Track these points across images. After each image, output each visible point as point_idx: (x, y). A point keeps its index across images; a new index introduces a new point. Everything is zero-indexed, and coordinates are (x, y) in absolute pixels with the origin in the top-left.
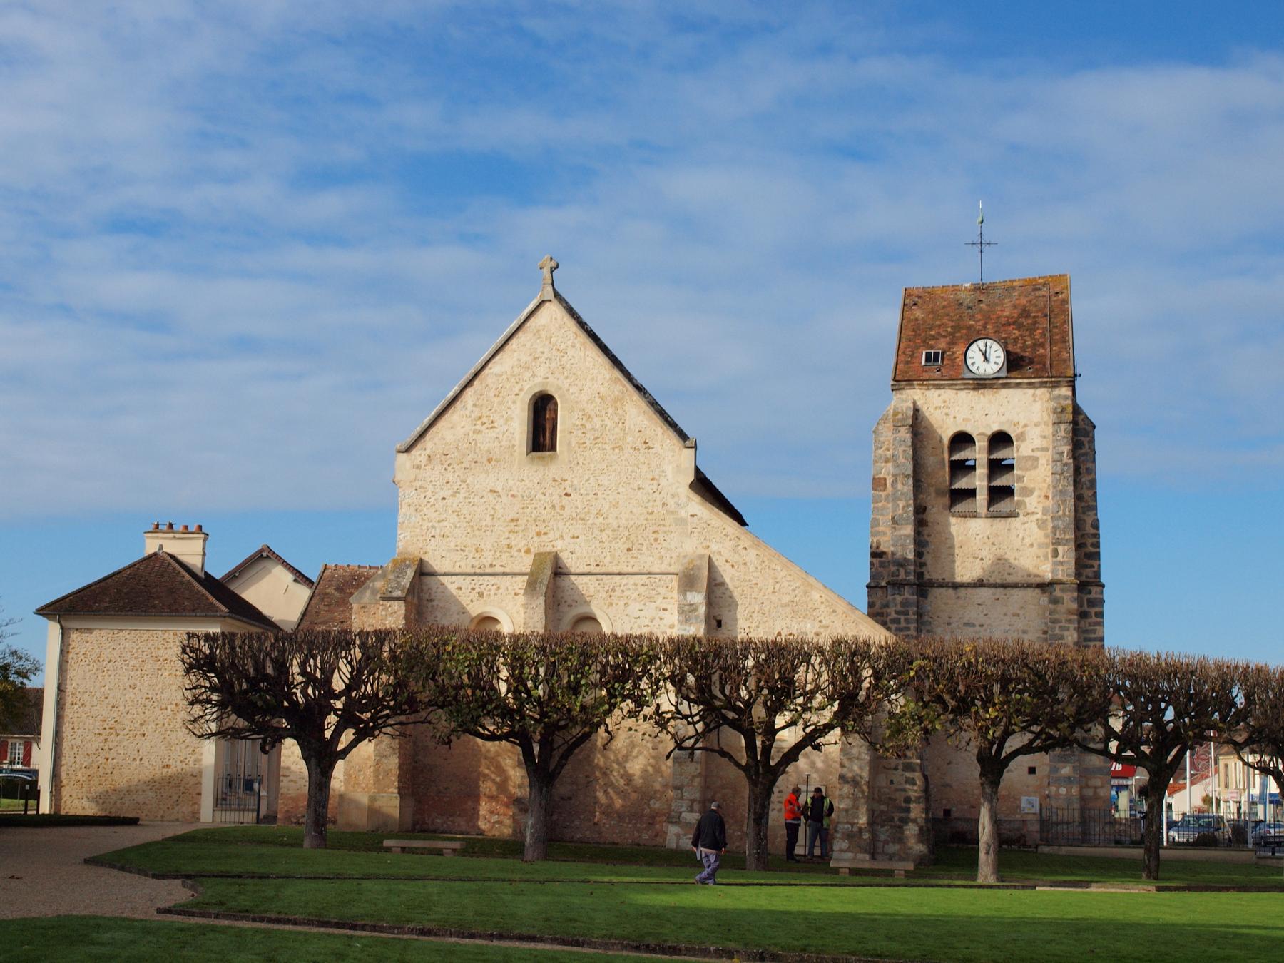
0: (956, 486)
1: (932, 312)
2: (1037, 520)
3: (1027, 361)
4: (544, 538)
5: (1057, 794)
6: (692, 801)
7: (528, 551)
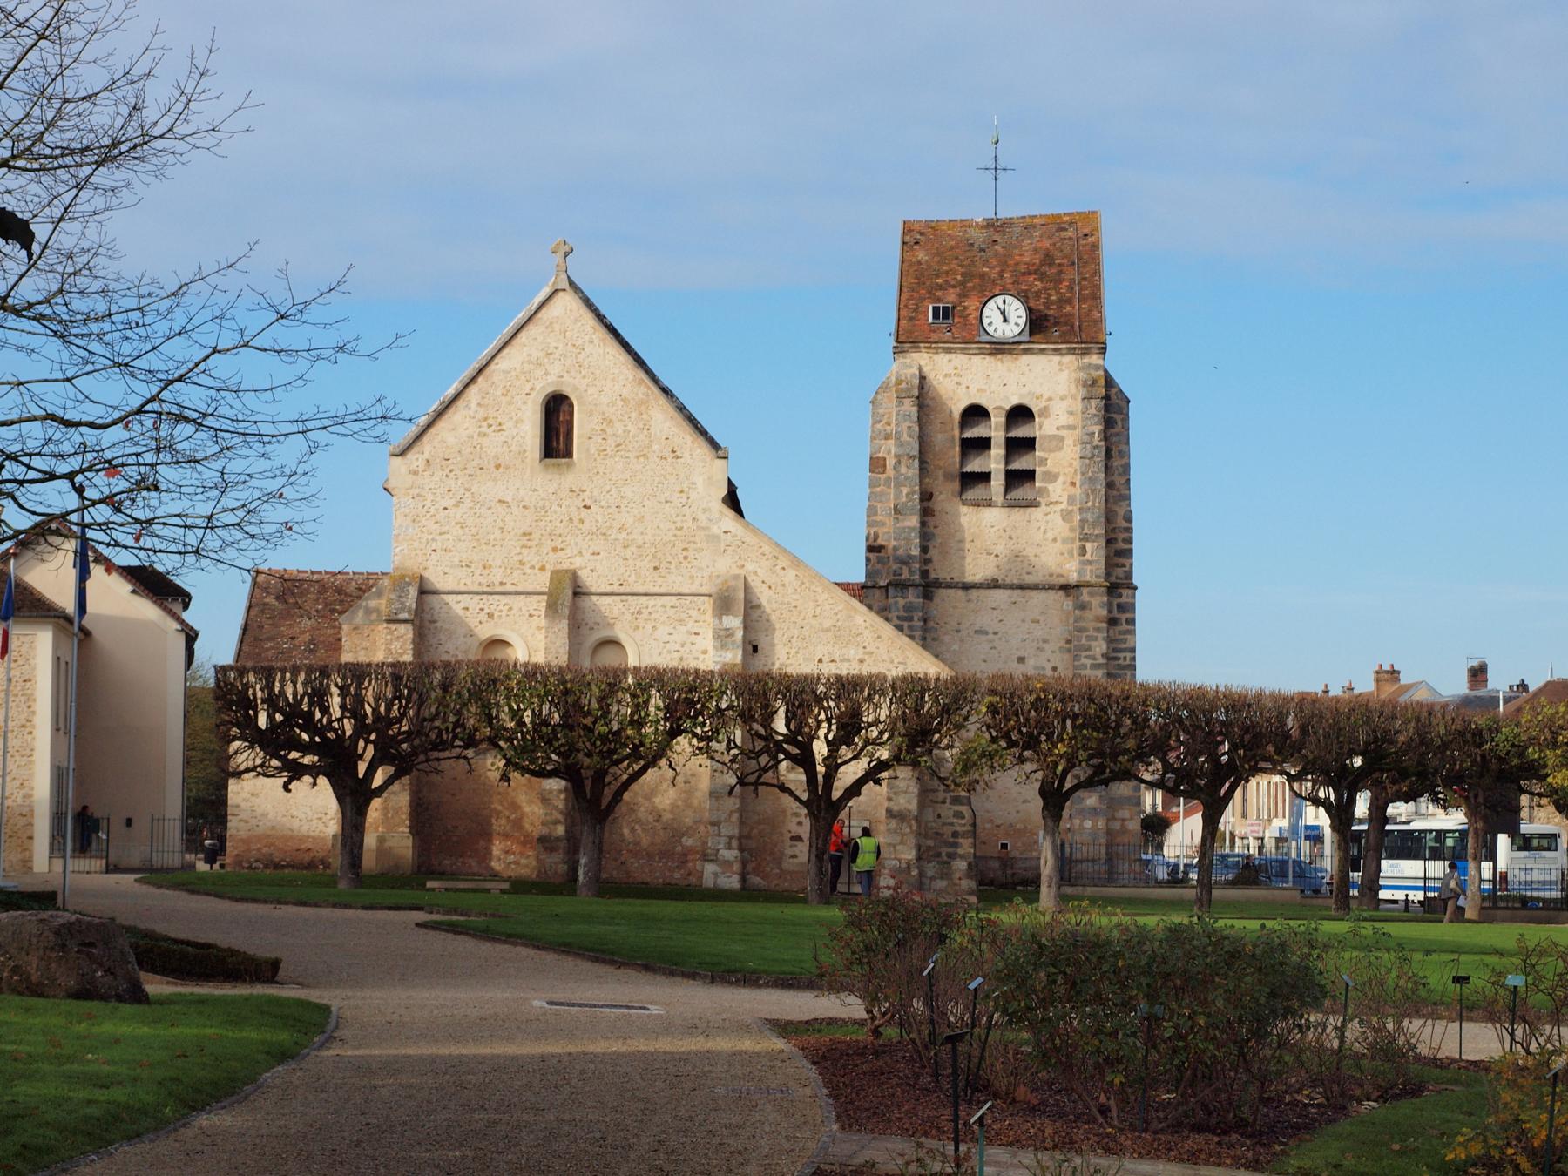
0: (968, 469)
1: (938, 254)
3: (1052, 321)
4: (560, 554)
6: (731, 838)
7: (543, 568)
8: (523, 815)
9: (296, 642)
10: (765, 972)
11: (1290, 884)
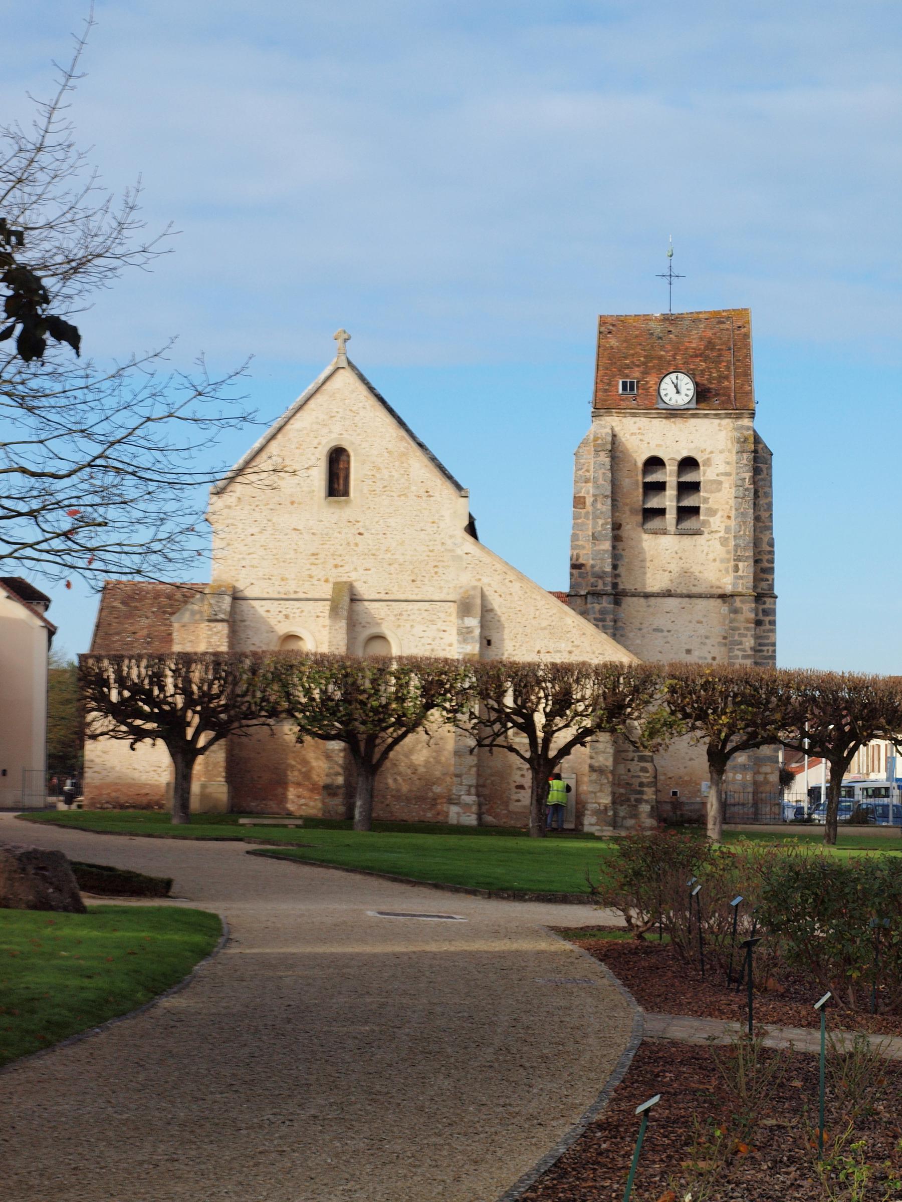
0: (649, 505)
1: (625, 341)
2: (720, 538)
4: (340, 570)
5: (734, 780)
6: (470, 786)
8: (311, 769)
9: (137, 636)
10: (529, 890)
11: (891, 824)
